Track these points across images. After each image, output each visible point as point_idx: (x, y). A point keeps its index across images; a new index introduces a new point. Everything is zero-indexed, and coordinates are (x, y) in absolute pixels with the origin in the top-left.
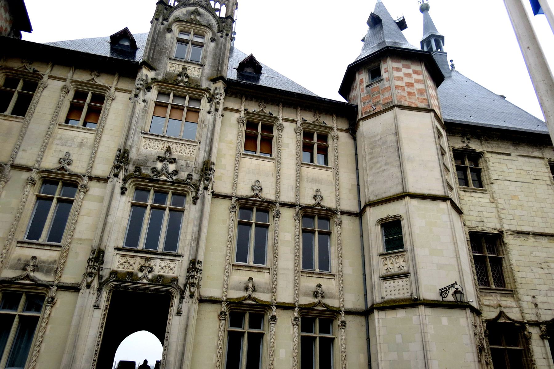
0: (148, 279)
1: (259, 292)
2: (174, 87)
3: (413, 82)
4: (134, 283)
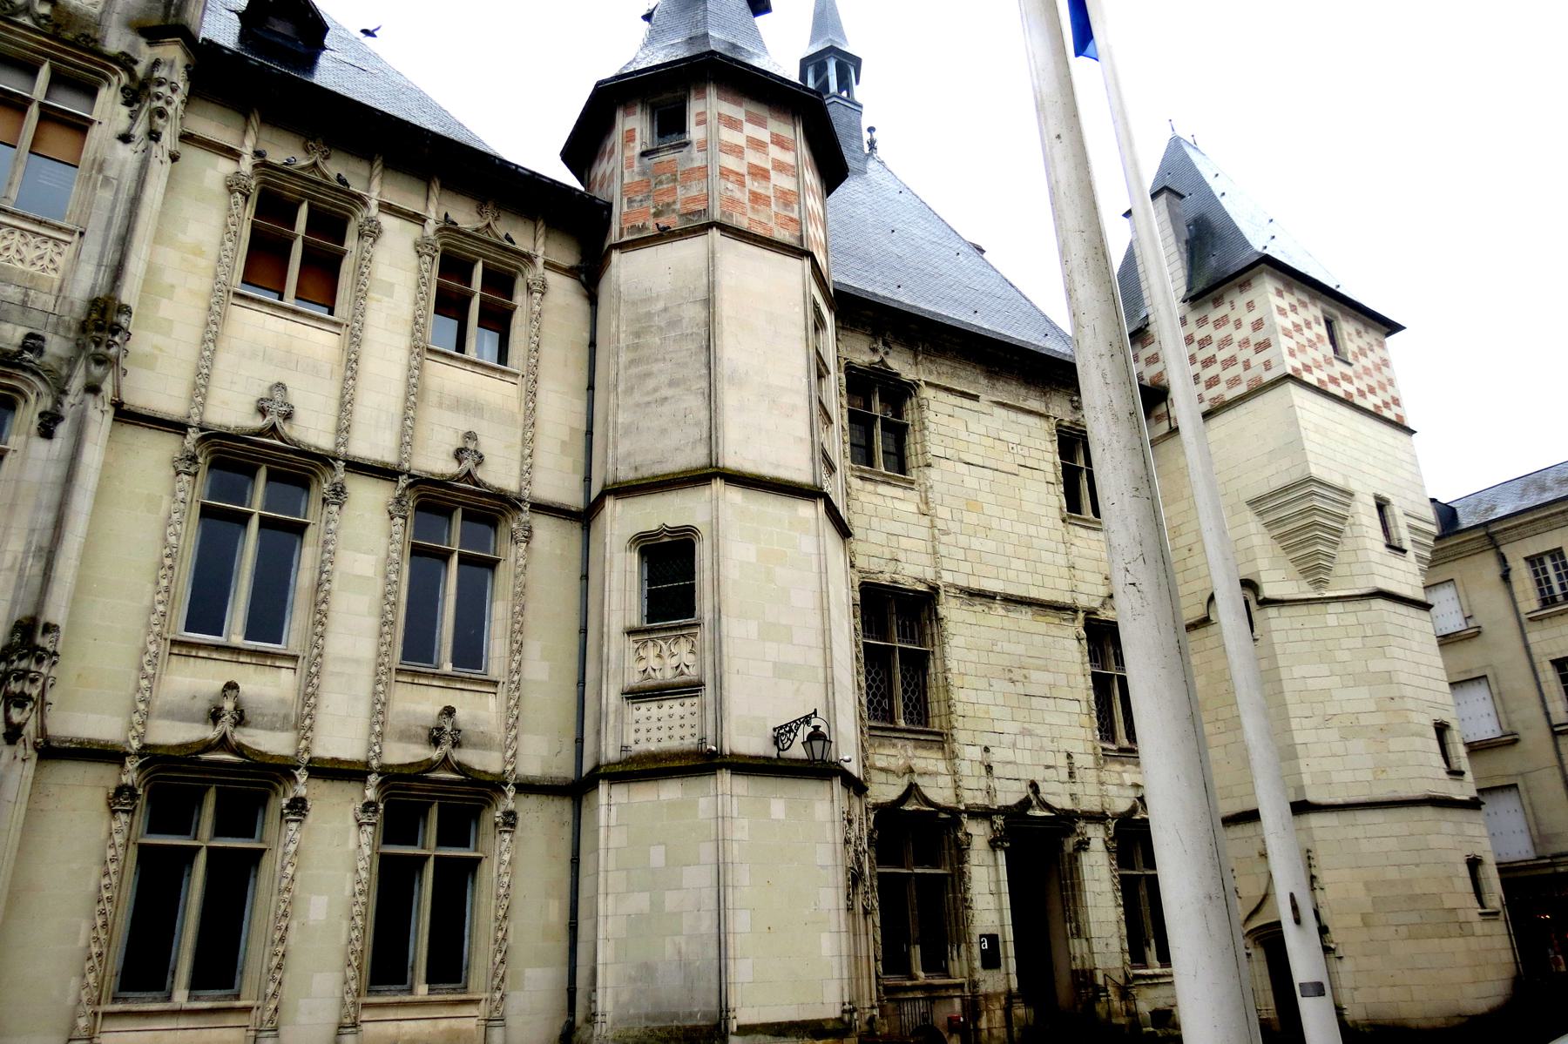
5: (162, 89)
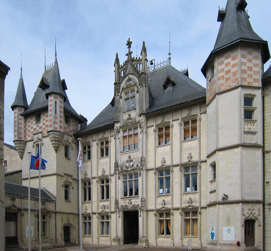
1: (168, 205)
4: (127, 208)
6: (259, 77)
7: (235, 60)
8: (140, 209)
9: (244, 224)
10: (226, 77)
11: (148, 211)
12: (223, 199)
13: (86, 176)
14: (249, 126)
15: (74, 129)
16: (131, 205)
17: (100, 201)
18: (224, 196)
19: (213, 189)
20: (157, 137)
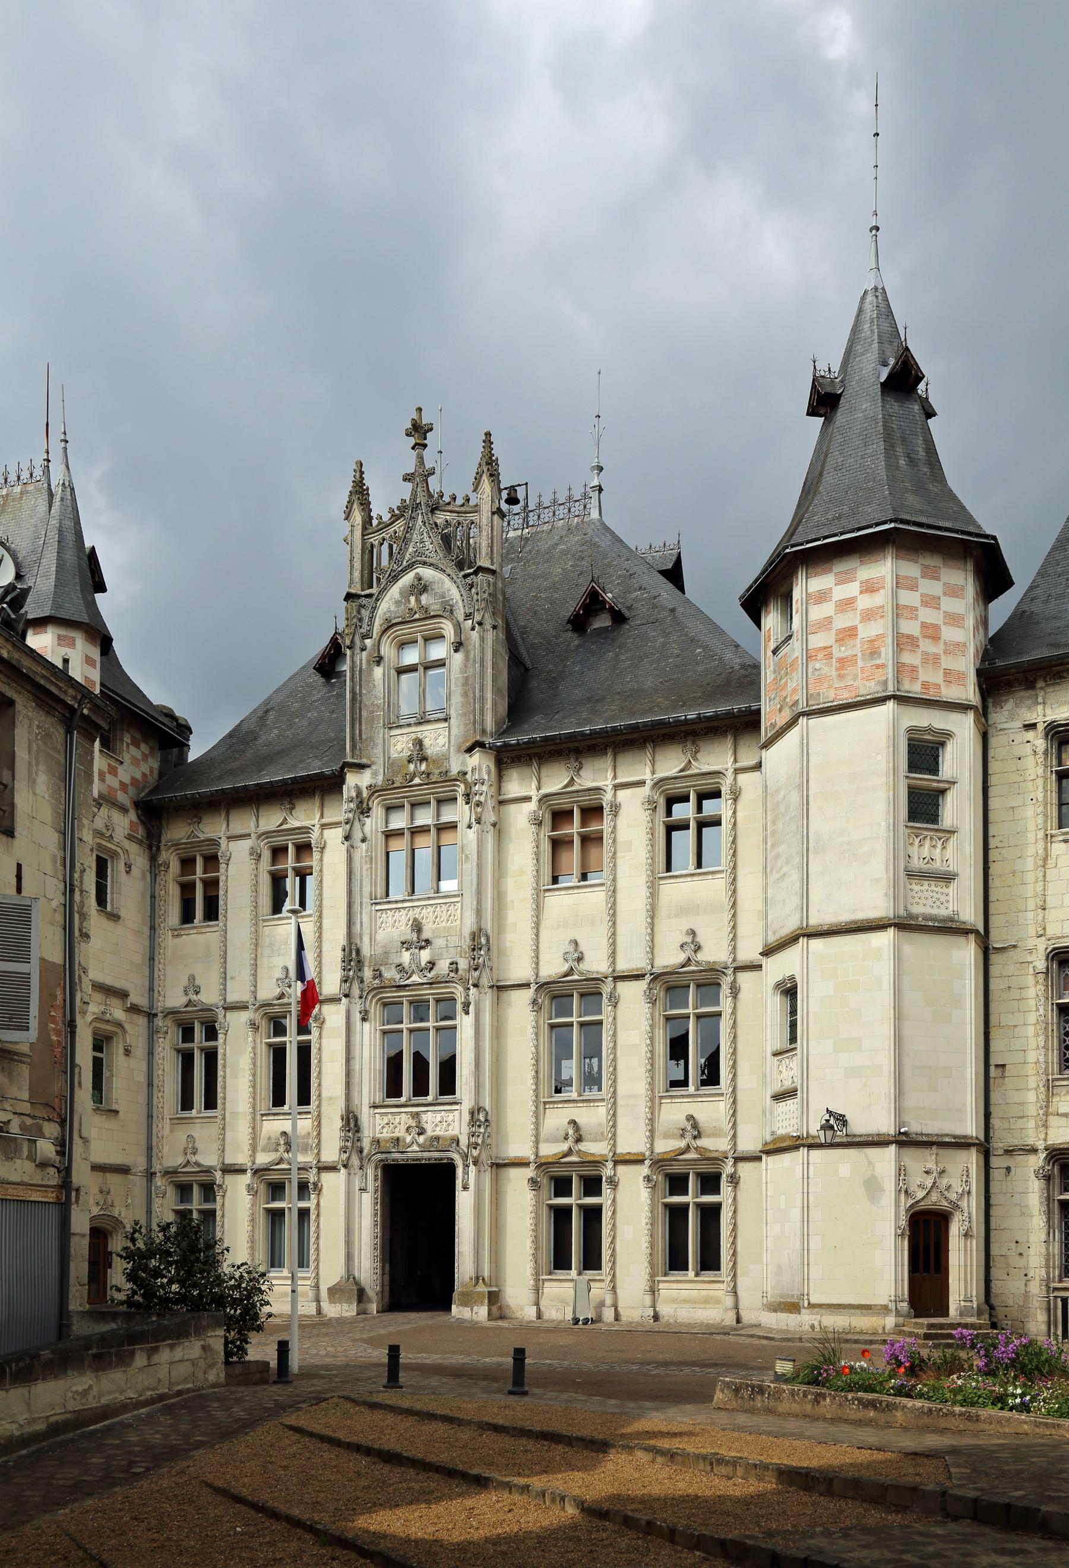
0: (419, 1145)
2: (406, 792)
3: (856, 622)
4: (402, 1152)
5: (477, 787)
6: (967, 664)
7: (872, 592)
8: (465, 1157)
9: (907, 1229)
10: (838, 652)
11: (499, 1166)
12: (827, 1127)
13: (194, 997)
14: (926, 851)
15: (138, 776)
16: (421, 1139)
17: (262, 1115)
18: (827, 1117)
19: (788, 1084)
20: (546, 847)
